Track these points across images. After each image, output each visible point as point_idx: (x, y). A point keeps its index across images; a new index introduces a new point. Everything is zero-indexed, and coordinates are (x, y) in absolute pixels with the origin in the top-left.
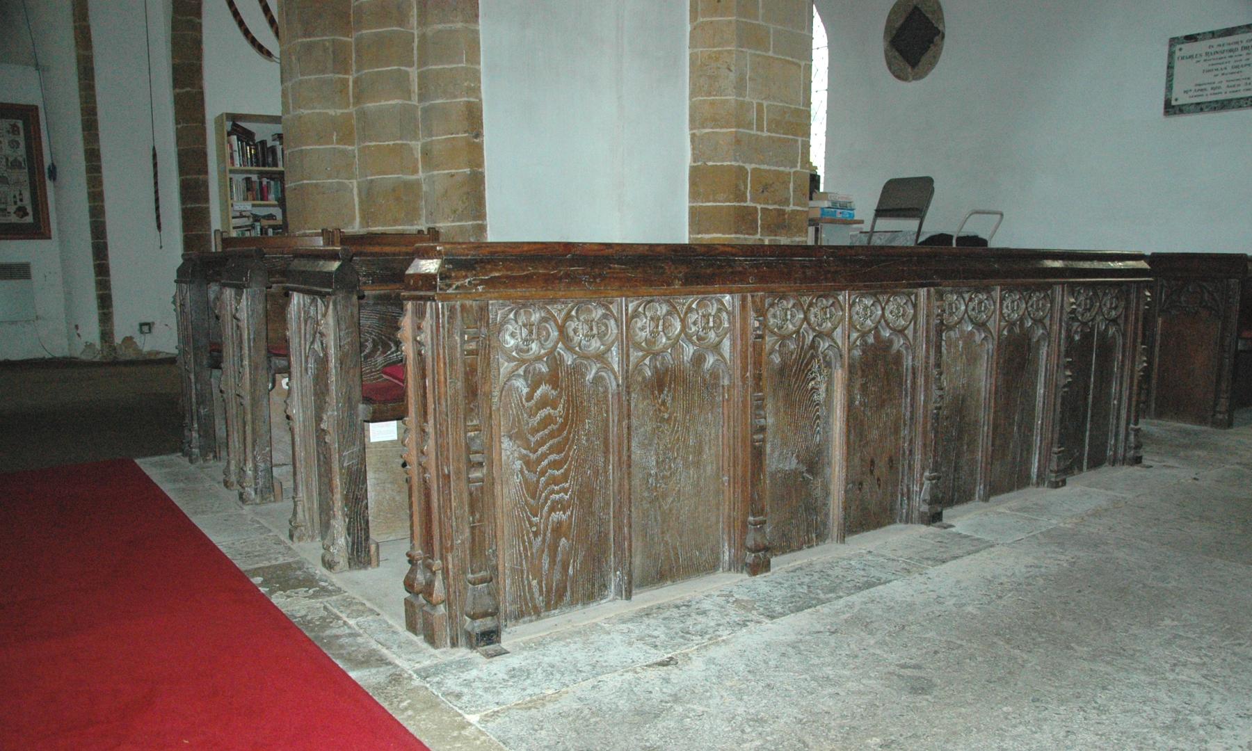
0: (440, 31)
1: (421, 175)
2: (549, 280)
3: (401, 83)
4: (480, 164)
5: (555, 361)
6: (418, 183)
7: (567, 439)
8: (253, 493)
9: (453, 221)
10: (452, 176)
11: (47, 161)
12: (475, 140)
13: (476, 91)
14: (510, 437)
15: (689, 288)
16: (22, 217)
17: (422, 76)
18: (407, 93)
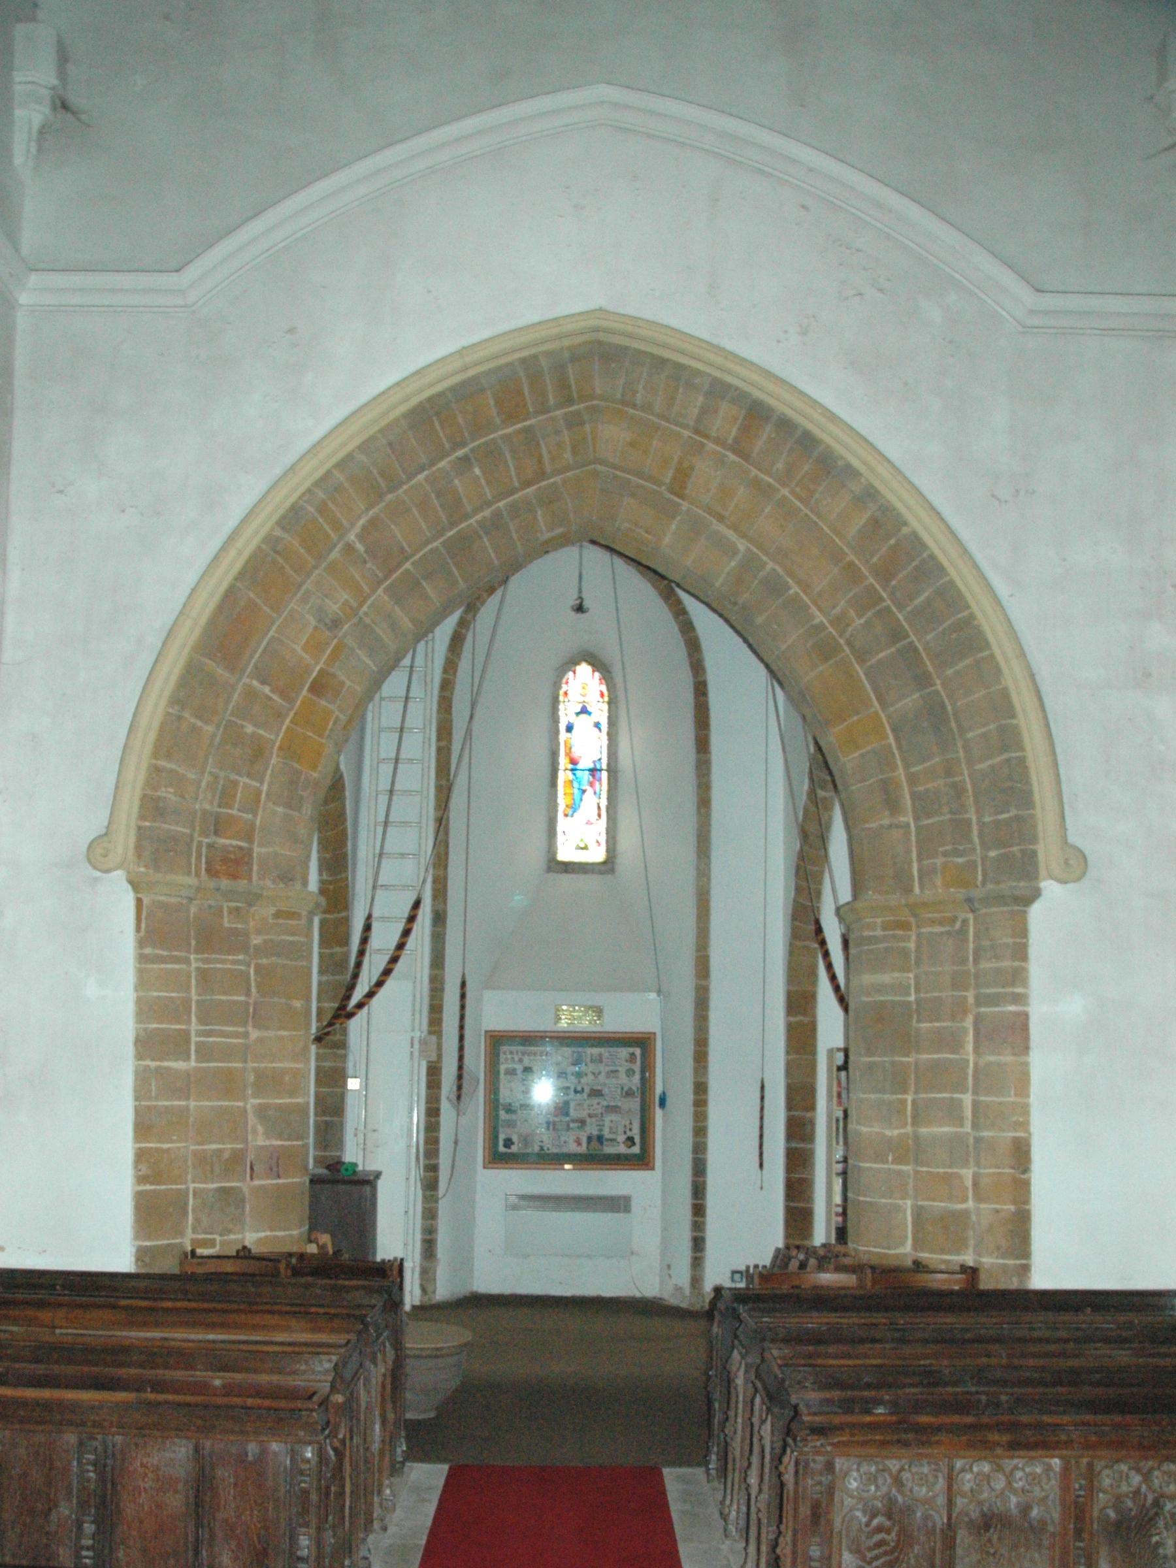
0: (991, 1063)
1: (970, 1204)
2: (883, 1444)
3: (953, 1112)
4: (1027, 1201)
5: (891, 1501)
6: (966, 1213)
7: (897, 1558)
8: (734, 1530)
9: (997, 1258)
10: (997, 1211)
11: (659, 1090)
12: (1022, 1176)
13: (1025, 1125)
14: (851, 1551)
15: (1012, 1453)
16: (630, 1147)
17: (975, 1104)
18: (960, 1122)
